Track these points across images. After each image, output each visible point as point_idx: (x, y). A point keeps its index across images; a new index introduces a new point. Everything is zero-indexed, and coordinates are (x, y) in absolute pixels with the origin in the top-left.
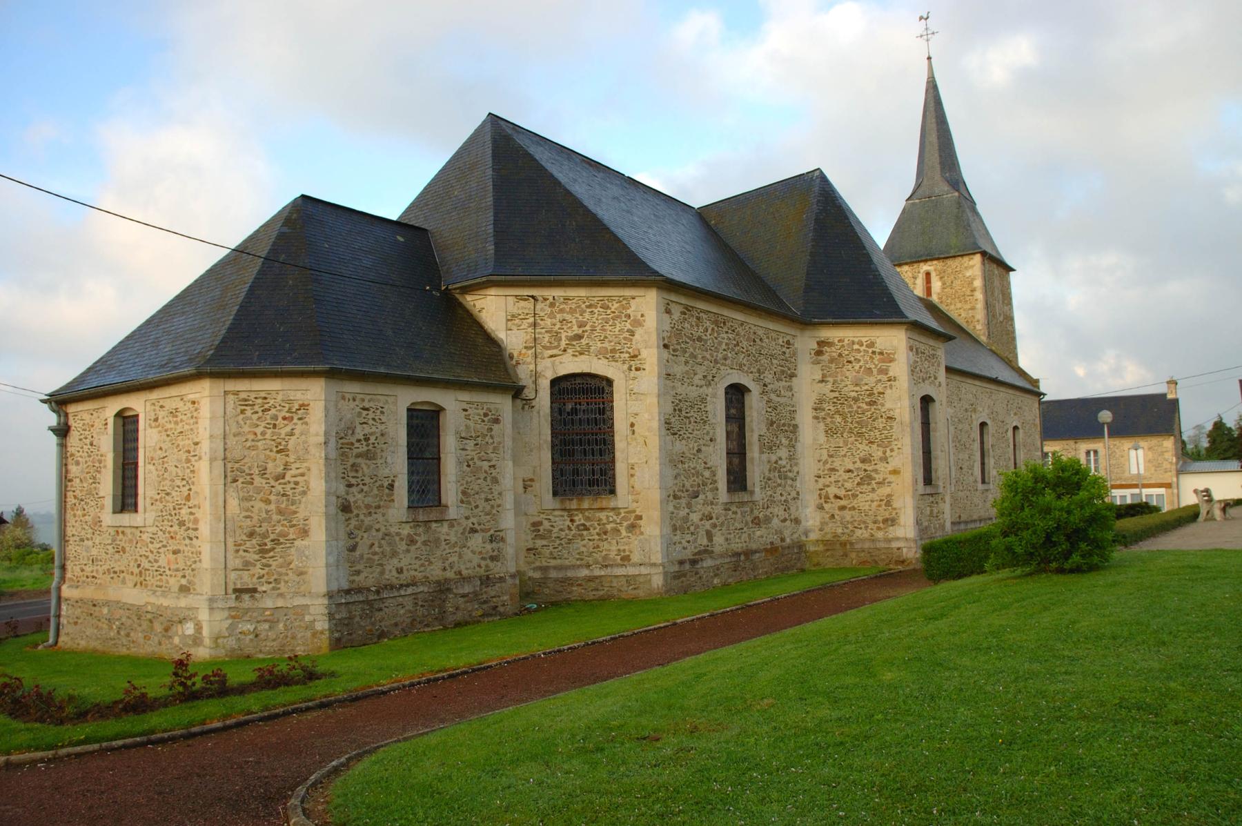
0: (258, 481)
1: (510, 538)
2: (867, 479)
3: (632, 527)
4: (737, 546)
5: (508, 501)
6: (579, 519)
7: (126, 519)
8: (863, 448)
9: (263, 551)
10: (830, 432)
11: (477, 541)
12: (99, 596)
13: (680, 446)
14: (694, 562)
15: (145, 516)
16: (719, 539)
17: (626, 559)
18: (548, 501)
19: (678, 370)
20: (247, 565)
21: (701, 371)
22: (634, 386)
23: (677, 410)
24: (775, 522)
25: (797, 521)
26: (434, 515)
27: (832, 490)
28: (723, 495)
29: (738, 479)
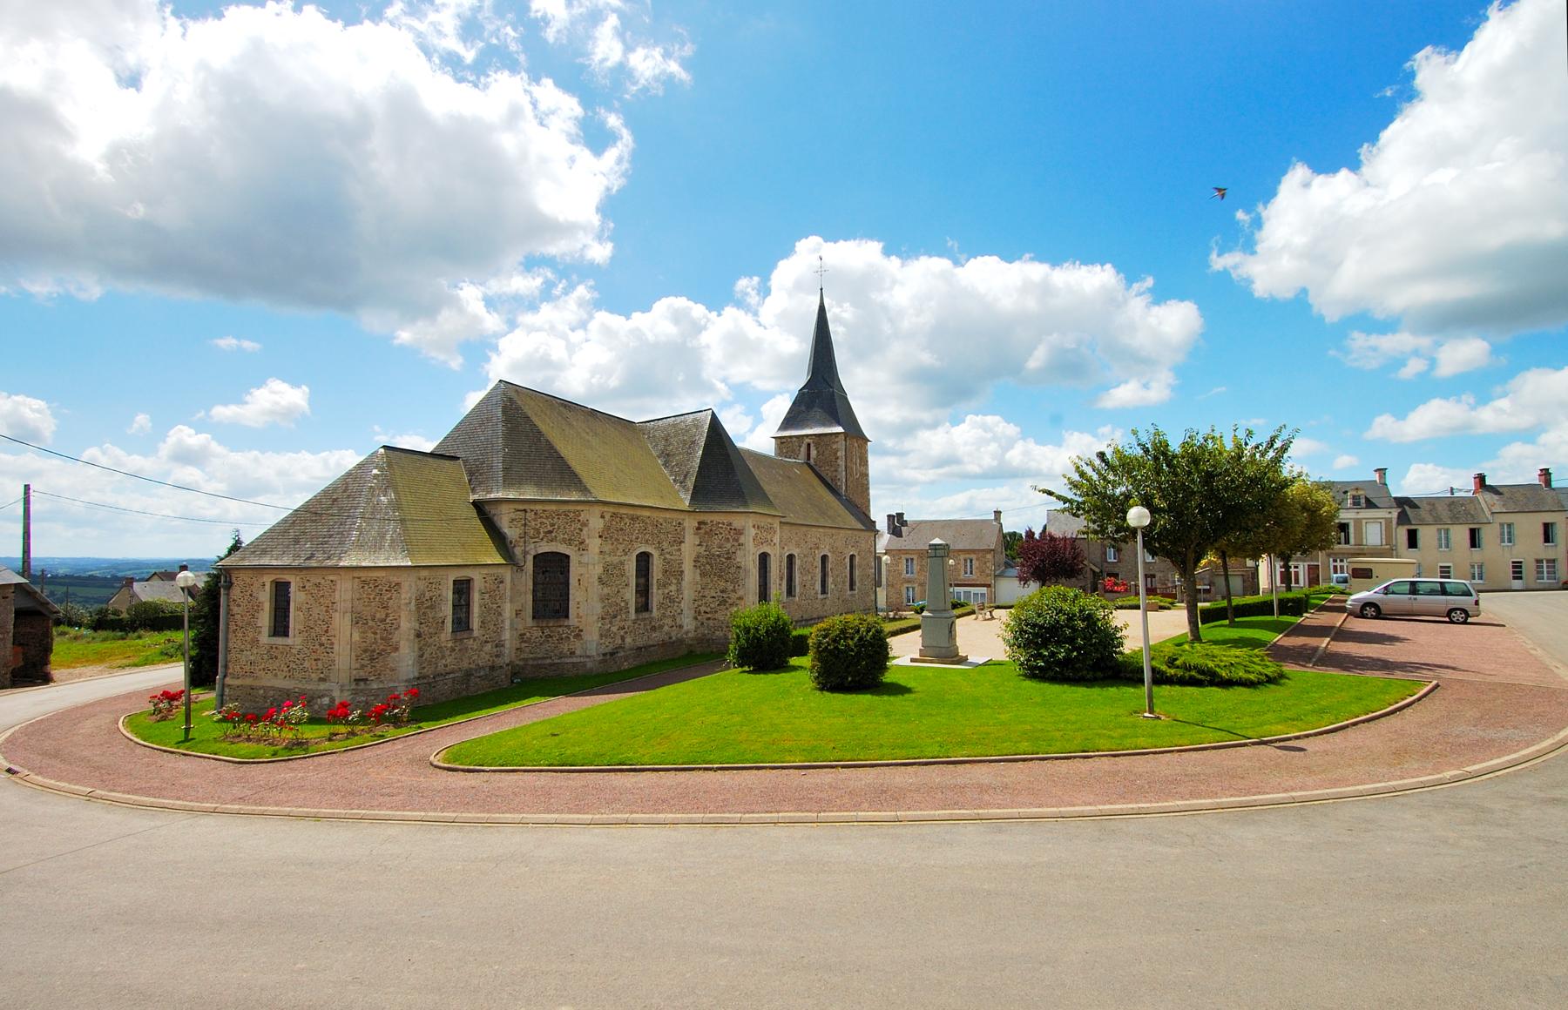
0: (371, 623)
1: (507, 644)
2: (723, 602)
3: (578, 636)
4: (640, 643)
5: (507, 623)
6: (547, 632)
7: (279, 641)
8: (722, 584)
9: (372, 660)
10: (703, 575)
11: (488, 647)
12: (256, 683)
13: (606, 590)
14: (612, 654)
15: (294, 639)
16: (628, 640)
17: (573, 653)
18: (530, 621)
19: (607, 548)
20: (363, 666)
21: (621, 547)
22: (585, 559)
23: (606, 570)
24: (666, 628)
25: (681, 627)
26: (465, 635)
27: (703, 609)
28: (633, 616)
29: (644, 607)
